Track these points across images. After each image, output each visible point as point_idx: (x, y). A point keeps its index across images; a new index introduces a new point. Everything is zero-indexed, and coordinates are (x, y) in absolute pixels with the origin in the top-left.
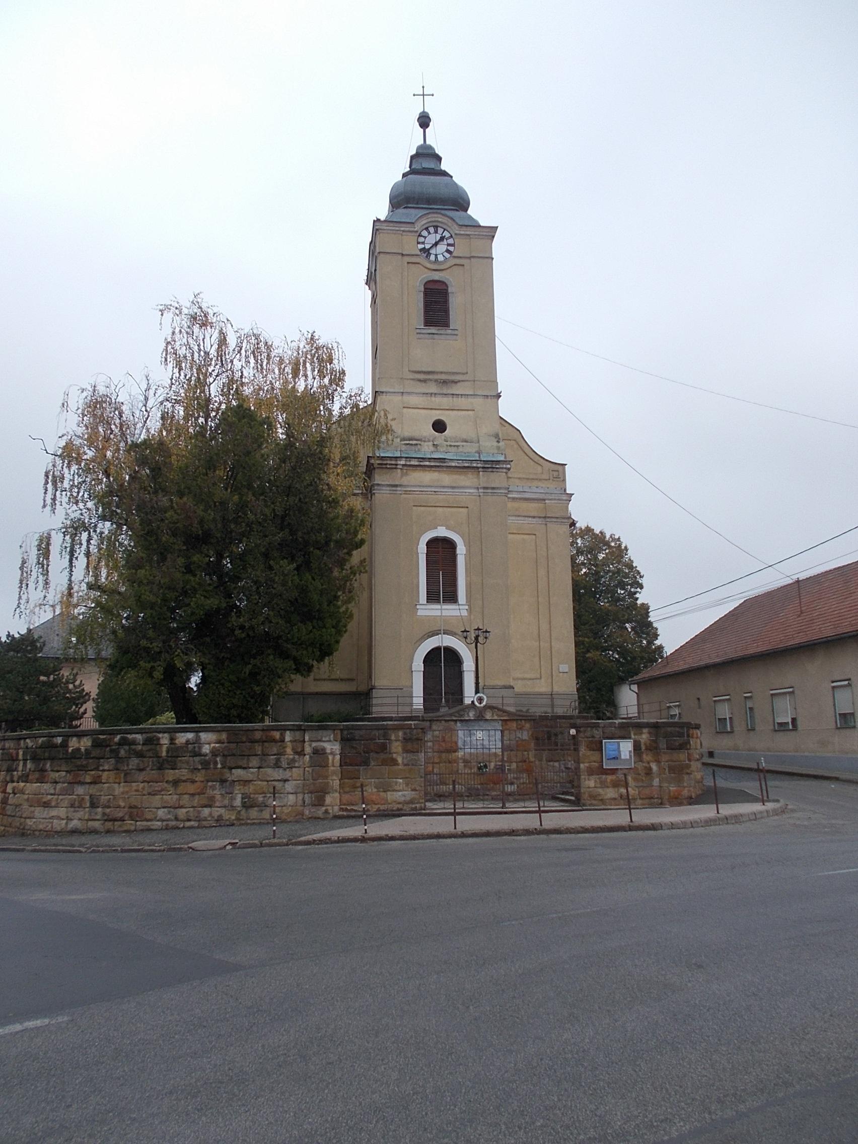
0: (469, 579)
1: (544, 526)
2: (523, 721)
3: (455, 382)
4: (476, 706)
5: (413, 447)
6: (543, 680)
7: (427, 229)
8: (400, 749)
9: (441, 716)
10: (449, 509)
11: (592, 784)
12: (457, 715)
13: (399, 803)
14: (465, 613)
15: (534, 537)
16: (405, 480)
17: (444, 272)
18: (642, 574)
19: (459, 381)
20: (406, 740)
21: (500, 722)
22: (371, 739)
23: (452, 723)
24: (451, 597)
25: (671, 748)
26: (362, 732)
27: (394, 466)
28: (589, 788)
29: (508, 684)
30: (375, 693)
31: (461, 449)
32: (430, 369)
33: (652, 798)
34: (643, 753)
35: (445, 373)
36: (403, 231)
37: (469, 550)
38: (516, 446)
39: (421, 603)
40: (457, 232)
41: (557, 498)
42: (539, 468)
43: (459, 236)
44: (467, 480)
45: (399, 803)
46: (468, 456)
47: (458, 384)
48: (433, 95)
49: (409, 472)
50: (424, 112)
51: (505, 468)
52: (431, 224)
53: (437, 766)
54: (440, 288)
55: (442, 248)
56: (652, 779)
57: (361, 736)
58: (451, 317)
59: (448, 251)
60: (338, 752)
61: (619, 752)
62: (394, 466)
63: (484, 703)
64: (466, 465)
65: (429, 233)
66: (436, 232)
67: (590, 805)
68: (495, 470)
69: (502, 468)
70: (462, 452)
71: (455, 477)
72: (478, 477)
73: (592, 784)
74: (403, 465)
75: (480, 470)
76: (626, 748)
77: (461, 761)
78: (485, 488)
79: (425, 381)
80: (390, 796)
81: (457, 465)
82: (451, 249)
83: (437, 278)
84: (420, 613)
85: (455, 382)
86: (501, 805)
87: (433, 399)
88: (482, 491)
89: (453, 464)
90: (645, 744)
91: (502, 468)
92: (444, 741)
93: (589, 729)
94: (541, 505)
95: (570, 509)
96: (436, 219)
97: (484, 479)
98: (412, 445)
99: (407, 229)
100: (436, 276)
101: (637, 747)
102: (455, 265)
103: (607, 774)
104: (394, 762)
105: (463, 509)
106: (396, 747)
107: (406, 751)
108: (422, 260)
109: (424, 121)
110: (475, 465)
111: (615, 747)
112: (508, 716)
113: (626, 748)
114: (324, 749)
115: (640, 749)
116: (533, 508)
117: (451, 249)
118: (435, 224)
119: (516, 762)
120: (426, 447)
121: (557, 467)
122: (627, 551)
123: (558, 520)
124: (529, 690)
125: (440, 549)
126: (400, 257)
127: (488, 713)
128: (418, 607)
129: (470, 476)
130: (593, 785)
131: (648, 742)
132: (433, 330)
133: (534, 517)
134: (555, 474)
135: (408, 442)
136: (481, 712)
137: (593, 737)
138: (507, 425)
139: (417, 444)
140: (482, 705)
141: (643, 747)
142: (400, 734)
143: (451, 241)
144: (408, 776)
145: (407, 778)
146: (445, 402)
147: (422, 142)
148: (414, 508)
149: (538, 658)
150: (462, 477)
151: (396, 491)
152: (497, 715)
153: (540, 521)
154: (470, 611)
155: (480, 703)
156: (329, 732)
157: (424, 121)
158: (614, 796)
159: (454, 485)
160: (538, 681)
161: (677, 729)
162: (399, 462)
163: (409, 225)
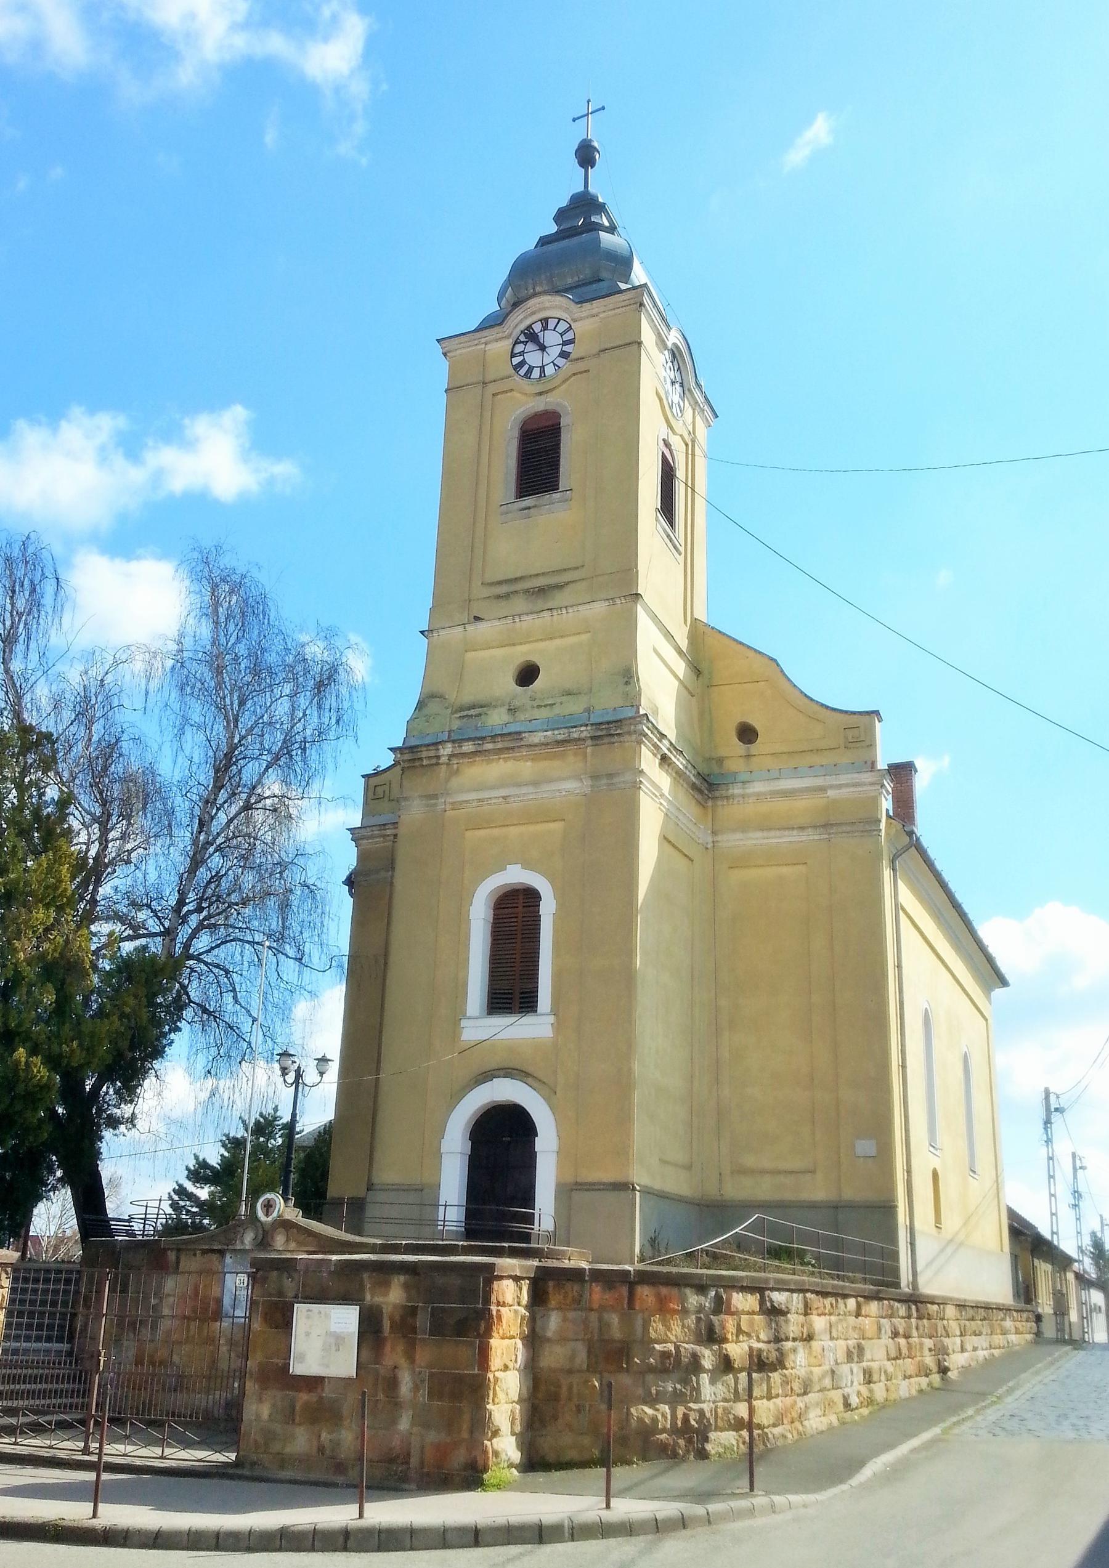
19: (567, 583)
24: (526, 1003)
25: (437, 1329)
32: (518, 575)
37: (561, 906)
48: (603, 108)
58: (561, 469)
63: (275, 1214)
73: (265, 1411)
79: (507, 596)
86: (82, 1445)
90: (391, 1319)
98: (471, 716)
100: (539, 405)
109: (586, 156)
124: (788, 1196)
132: (529, 501)
134: (850, 734)
135: (465, 713)
136: (265, 1233)
138: (751, 654)
141: (386, 1324)
147: (582, 189)
150: (556, 763)
154: (558, 1027)
157: (586, 156)
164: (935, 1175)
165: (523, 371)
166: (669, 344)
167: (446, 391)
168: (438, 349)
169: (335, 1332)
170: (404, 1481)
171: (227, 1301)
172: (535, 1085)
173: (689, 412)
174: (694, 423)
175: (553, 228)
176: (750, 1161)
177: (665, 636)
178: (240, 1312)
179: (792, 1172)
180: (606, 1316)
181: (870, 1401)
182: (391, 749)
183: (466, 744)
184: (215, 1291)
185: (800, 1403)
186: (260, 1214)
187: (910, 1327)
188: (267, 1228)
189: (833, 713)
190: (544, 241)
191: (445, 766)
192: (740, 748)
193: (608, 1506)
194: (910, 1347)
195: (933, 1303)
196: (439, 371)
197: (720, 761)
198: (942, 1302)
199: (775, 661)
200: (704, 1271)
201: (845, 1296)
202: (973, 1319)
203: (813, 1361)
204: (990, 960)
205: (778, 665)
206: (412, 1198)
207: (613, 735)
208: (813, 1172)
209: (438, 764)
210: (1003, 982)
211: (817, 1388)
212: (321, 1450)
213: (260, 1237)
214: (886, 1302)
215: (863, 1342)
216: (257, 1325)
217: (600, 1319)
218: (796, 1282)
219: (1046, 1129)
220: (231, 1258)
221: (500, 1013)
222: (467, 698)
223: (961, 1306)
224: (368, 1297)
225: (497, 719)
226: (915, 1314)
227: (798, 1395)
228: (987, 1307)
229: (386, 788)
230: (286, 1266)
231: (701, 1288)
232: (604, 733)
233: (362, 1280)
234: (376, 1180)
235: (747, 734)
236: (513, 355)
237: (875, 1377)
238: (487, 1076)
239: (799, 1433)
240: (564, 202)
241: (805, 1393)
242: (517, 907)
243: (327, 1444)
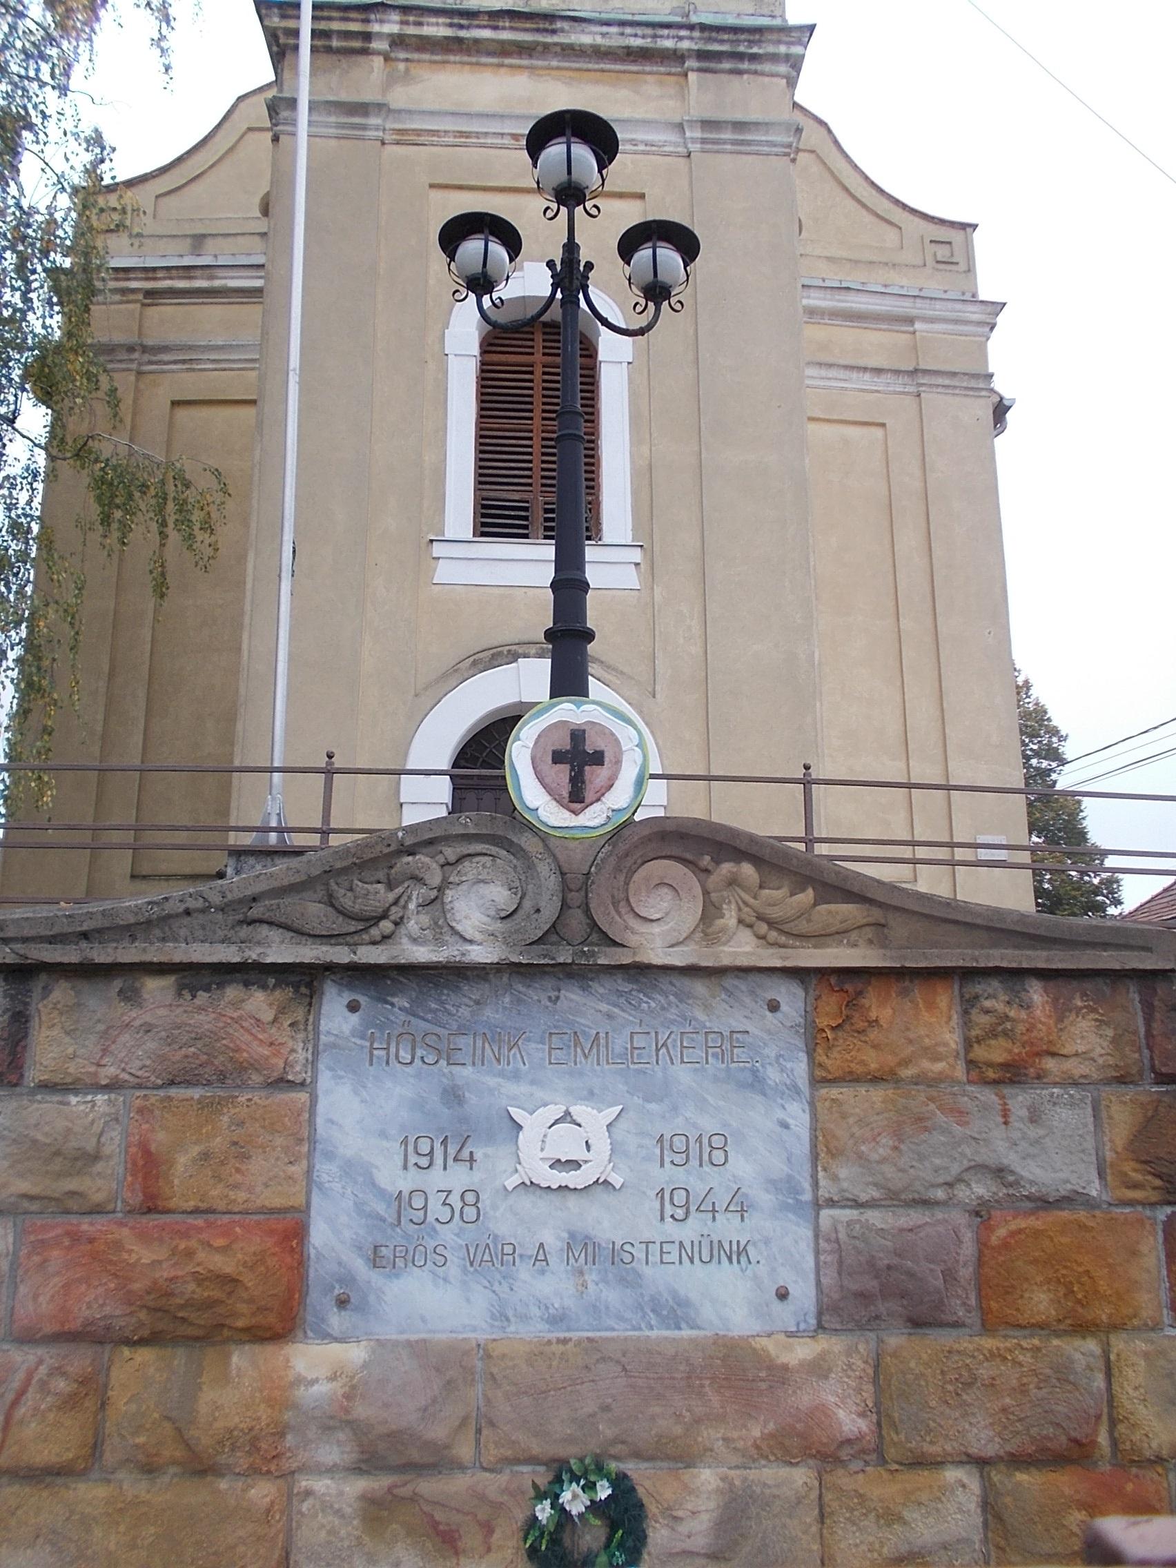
0: (645, 450)
1: (909, 401)
2: (1036, 993)
9: (131, 931)
12: (314, 911)
15: (879, 432)
16: (399, 97)
18: (1063, 733)
21: (792, 998)
23: (259, 1003)
27: (357, 44)
42: (891, 235)
49: (416, 70)
62: (357, 44)
68: (745, 65)
72: (682, 94)
74: (398, 41)
75: (691, 63)
77: (331, 1452)
78: (707, 124)
84: (445, 573)
92: (151, 1206)
94: (903, 339)
95: (992, 345)
112: (879, 933)
119: (981, 1463)
122: (1028, 689)
123: (955, 382)
127: (656, 904)
133: (878, 371)
134: (943, 253)
140: (594, 817)
149: (903, 814)
150: (623, 93)
153: (898, 384)
154: (650, 569)
155: (576, 797)
162: (376, 28)
169: (1084, 1338)
183: (434, 20)
191: (381, 59)
205: (830, 131)
209: (365, 52)
220: (353, 1007)
232: (725, 48)
238: (500, 653)
242: (532, 354)
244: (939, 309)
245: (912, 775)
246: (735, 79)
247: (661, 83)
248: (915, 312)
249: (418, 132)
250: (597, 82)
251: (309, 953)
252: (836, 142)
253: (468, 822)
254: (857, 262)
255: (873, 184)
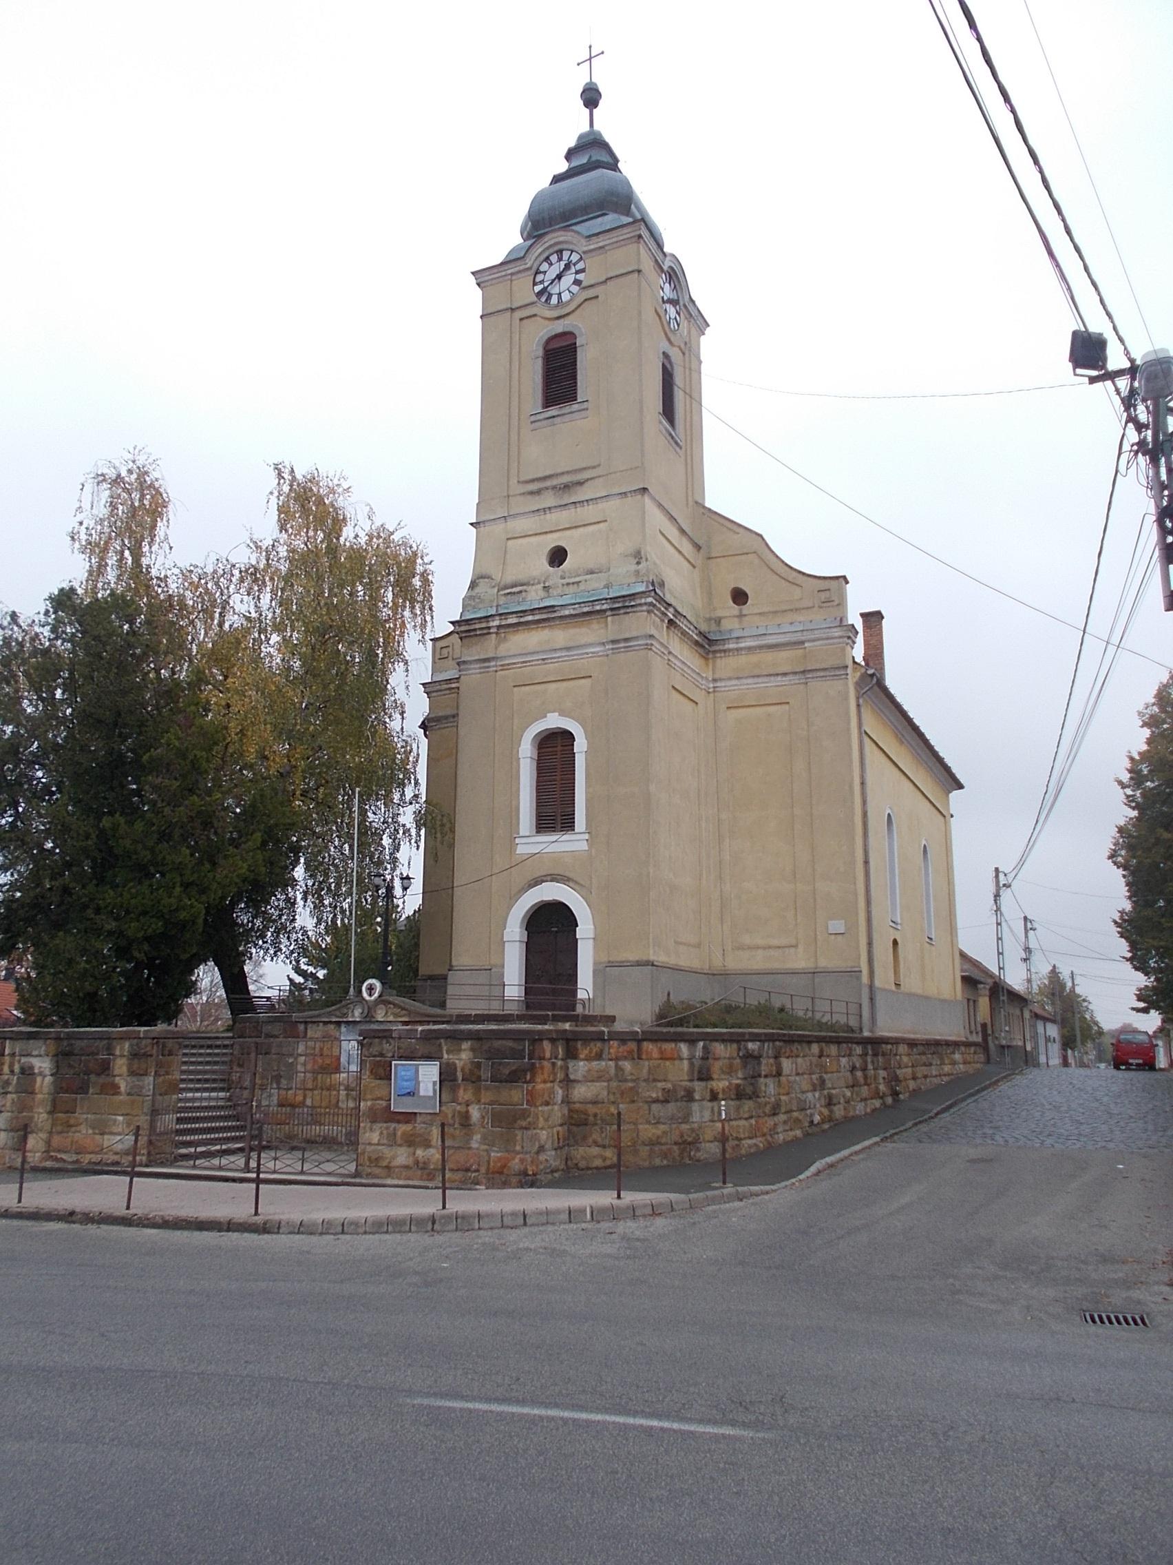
3: (580, 483)
4: (364, 999)
5: (515, 598)
6: (801, 949)
7: (547, 259)
8: (125, 1069)
10: (565, 684)
11: (375, 1137)
13: (116, 1153)
14: (584, 846)
15: (786, 707)
16: (503, 650)
17: (571, 317)
19: (588, 480)
20: (135, 1055)
22: (93, 1054)
23: (332, 1026)
24: (567, 824)
26: (84, 1043)
27: (485, 631)
28: (370, 1144)
29: (645, 958)
30: (452, 977)
31: (582, 587)
32: (548, 473)
33: (467, 1170)
34: (459, 1086)
35: (568, 472)
36: (512, 274)
38: (757, 561)
39: (521, 834)
40: (585, 249)
41: (824, 636)
42: (797, 593)
43: (589, 254)
44: (591, 634)
45: (116, 1153)
46: (592, 596)
47: (586, 485)
48: (603, 53)
50: (591, 83)
51: (646, 604)
52: (551, 250)
53: (309, 1094)
54: (565, 344)
55: (568, 279)
56: (469, 1136)
57: (82, 1049)
59: (577, 282)
60: (47, 1072)
61: (418, 1083)
62: (485, 631)
64: (586, 610)
65: (551, 264)
66: (560, 259)
67: (369, 1175)
69: (640, 605)
70: (584, 591)
71: (572, 631)
73: (375, 1137)
74: (499, 627)
76: (428, 1075)
78: (613, 642)
79: (538, 492)
80: (108, 1140)
81: (572, 612)
82: (580, 277)
83: (560, 330)
84: (522, 849)
85: (580, 483)
87: (548, 516)
88: (611, 647)
89: (567, 612)
90: (463, 1070)
91: (640, 605)
93: (377, 1040)
96: (556, 240)
97: (613, 627)
98: (514, 593)
99: (517, 269)
100: (559, 327)
101: (447, 1077)
102: (586, 300)
103: (399, 1122)
104: (115, 1090)
105: (583, 681)
106: (120, 1066)
107: (132, 1073)
108: (540, 309)
109: (591, 97)
110: (598, 608)
111: (410, 1074)
112: (409, 1015)
113: (428, 1075)
114: (32, 1068)
115: (455, 1080)
116: (784, 660)
117: (580, 277)
118: (556, 248)
120: (533, 593)
121: (826, 584)
124: (776, 966)
125: (559, 748)
126: (508, 314)
128: (517, 841)
129: (595, 626)
130: (375, 1141)
131: (469, 1066)
132: (553, 411)
133: (785, 674)
134: (823, 596)
135: (509, 591)
137: (382, 1055)
138: (741, 530)
139: (521, 592)
140: (373, 998)
141: (460, 1075)
142: (127, 1045)
143: (580, 266)
144: (128, 1111)
145: (127, 1115)
146: (563, 517)
148: (516, 689)
150: (584, 630)
151: (488, 667)
152: (392, 1013)
156: (40, 1043)
157: (591, 97)
158: (406, 1163)
159: (572, 644)
160: (792, 950)
161: (510, 1044)
162: (491, 624)
163: (519, 263)
164: (895, 942)
165: (543, 299)
166: (665, 268)
167: (481, 317)
168: (472, 279)
170: (477, 1184)
171: (343, 1059)
172: (577, 887)
173: (684, 324)
174: (689, 332)
175: (563, 166)
176: (747, 940)
177: (669, 519)
178: (353, 1068)
179: (779, 947)
180: (620, 1063)
181: (830, 1119)
182: (451, 622)
184: (335, 1052)
185: (770, 1122)
186: (365, 995)
187: (866, 1062)
188: (370, 1004)
189: (809, 579)
190: (557, 179)
192: (735, 609)
193: (619, 1197)
194: (866, 1077)
195: (887, 1043)
196: (474, 299)
197: (718, 621)
198: (896, 1042)
199: (761, 536)
200: (695, 1030)
201: (809, 1042)
202: (924, 1054)
203: (782, 1091)
204: (947, 769)
205: (763, 539)
206: (482, 978)
207: (628, 607)
208: (796, 946)
209: (489, 633)
210: (960, 786)
211: (783, 1110)
212: (417, 1162)
213: (366, 1011)
214: (845, 1045)
215: (825, 1076)
216: (366, 1075)
217: (617, 1066)
218: (766, 1034)
219: (995, 901)
221: (545, 832)
222: (509, 578)
223: (912, 1044)
224: (446, 1056)
225: (535, 597)
226: (870, 1052)
227: (769, 1116)
228: (937, 1043)
229: (450, 649)
230: (385, 1035)
231: (692, 1041)
232: (620, 605)
233: (440, 1045)
234: (454, 963)
235: (739, 597)
236: (535, 284)
237: (835, 1101)
239: (769, 1143)
240: (572, 143)
241: (774, 1114)
243: (420, 1159)
244: (817, 634)
245: (584, 941)
246: (626, 617)
247: (598, 623)
248: (803, 638)
249: (508, 664)
250: (575, 627)
251: (337, 1020)
252: (767, 545)
253: (357, 999)
254: (776, 612)
255: (786, 565)
